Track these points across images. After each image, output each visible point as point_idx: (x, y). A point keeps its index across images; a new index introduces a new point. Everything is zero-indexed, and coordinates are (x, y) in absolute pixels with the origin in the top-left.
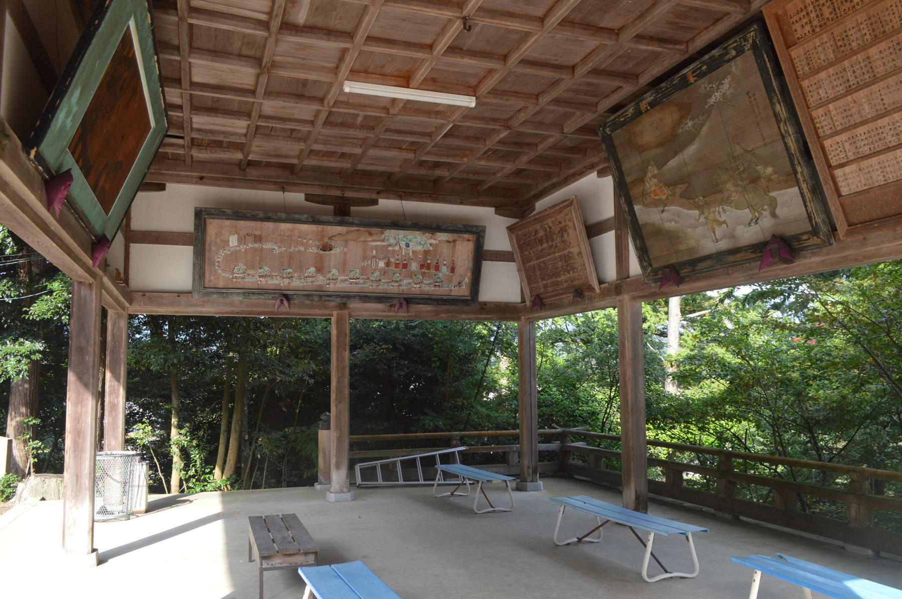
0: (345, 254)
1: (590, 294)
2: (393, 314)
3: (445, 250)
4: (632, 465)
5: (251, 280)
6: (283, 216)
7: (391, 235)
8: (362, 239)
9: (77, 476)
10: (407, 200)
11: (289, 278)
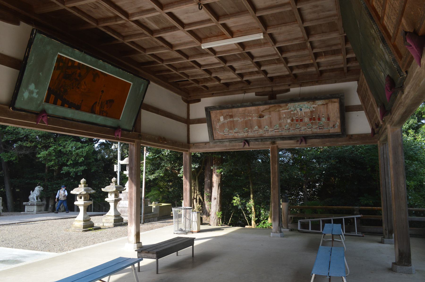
0: (270, 118)
3: (323, 109)
6: (239, 105)
7: (291, 106)
8: (277, 110)
10: (305, 86)
11: (247, 132)
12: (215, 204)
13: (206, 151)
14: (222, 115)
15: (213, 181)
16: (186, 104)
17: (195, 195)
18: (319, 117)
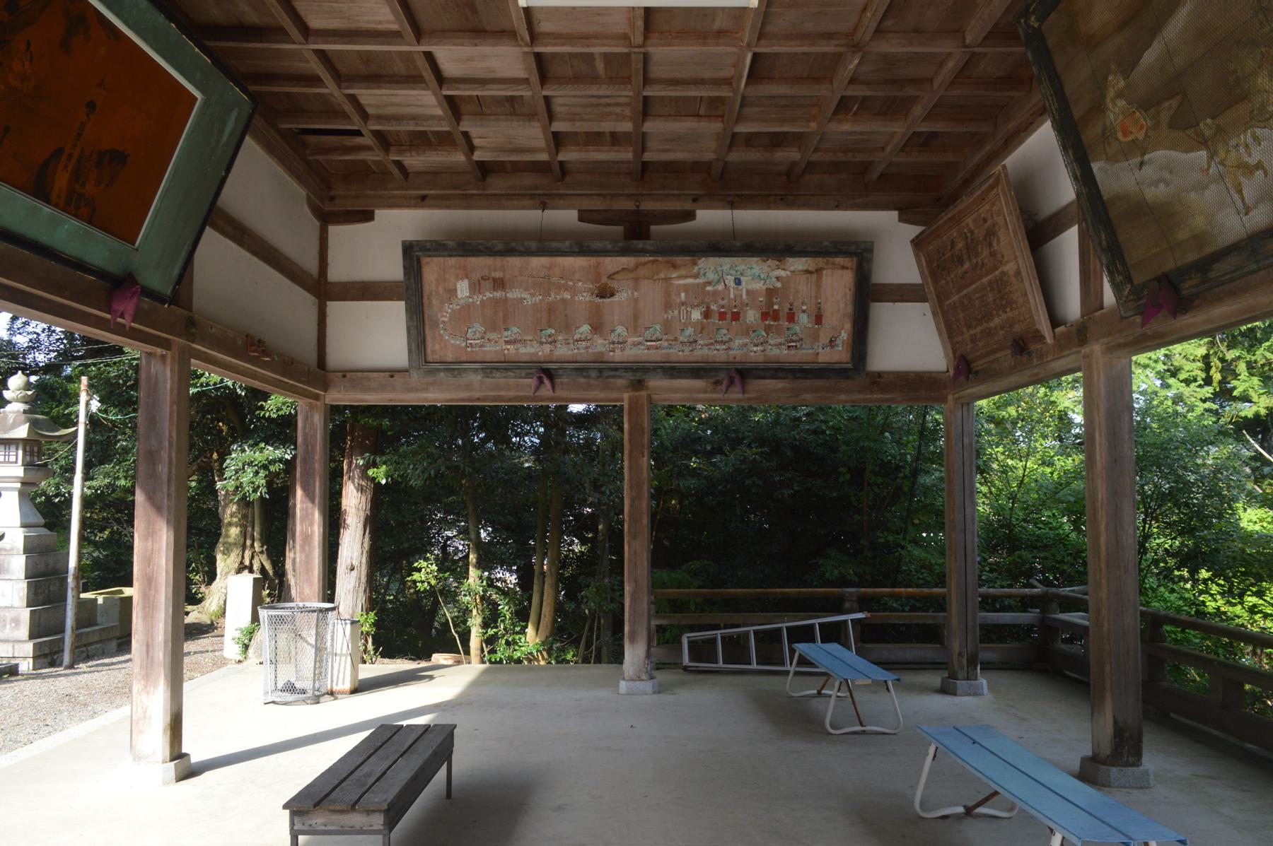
0: (636, 301)
1: (1038, 346)
2: (720, 396)
3: (804, 287)
4: (1107, 669)
5: (493, 349)
6: (533, 245)
7: (710, 267)
8: (662, 276)
9: (148, 645)
10: (744, 208)
11: (550, 343)
12: (353, 584)
13: (391, 400)
14: (467, 276)
15: (343, 508)
16: (317, 224)
17: (248, 554)
18: (790, 309)
